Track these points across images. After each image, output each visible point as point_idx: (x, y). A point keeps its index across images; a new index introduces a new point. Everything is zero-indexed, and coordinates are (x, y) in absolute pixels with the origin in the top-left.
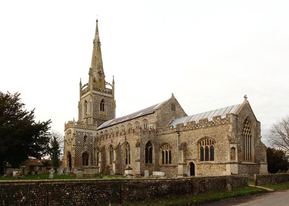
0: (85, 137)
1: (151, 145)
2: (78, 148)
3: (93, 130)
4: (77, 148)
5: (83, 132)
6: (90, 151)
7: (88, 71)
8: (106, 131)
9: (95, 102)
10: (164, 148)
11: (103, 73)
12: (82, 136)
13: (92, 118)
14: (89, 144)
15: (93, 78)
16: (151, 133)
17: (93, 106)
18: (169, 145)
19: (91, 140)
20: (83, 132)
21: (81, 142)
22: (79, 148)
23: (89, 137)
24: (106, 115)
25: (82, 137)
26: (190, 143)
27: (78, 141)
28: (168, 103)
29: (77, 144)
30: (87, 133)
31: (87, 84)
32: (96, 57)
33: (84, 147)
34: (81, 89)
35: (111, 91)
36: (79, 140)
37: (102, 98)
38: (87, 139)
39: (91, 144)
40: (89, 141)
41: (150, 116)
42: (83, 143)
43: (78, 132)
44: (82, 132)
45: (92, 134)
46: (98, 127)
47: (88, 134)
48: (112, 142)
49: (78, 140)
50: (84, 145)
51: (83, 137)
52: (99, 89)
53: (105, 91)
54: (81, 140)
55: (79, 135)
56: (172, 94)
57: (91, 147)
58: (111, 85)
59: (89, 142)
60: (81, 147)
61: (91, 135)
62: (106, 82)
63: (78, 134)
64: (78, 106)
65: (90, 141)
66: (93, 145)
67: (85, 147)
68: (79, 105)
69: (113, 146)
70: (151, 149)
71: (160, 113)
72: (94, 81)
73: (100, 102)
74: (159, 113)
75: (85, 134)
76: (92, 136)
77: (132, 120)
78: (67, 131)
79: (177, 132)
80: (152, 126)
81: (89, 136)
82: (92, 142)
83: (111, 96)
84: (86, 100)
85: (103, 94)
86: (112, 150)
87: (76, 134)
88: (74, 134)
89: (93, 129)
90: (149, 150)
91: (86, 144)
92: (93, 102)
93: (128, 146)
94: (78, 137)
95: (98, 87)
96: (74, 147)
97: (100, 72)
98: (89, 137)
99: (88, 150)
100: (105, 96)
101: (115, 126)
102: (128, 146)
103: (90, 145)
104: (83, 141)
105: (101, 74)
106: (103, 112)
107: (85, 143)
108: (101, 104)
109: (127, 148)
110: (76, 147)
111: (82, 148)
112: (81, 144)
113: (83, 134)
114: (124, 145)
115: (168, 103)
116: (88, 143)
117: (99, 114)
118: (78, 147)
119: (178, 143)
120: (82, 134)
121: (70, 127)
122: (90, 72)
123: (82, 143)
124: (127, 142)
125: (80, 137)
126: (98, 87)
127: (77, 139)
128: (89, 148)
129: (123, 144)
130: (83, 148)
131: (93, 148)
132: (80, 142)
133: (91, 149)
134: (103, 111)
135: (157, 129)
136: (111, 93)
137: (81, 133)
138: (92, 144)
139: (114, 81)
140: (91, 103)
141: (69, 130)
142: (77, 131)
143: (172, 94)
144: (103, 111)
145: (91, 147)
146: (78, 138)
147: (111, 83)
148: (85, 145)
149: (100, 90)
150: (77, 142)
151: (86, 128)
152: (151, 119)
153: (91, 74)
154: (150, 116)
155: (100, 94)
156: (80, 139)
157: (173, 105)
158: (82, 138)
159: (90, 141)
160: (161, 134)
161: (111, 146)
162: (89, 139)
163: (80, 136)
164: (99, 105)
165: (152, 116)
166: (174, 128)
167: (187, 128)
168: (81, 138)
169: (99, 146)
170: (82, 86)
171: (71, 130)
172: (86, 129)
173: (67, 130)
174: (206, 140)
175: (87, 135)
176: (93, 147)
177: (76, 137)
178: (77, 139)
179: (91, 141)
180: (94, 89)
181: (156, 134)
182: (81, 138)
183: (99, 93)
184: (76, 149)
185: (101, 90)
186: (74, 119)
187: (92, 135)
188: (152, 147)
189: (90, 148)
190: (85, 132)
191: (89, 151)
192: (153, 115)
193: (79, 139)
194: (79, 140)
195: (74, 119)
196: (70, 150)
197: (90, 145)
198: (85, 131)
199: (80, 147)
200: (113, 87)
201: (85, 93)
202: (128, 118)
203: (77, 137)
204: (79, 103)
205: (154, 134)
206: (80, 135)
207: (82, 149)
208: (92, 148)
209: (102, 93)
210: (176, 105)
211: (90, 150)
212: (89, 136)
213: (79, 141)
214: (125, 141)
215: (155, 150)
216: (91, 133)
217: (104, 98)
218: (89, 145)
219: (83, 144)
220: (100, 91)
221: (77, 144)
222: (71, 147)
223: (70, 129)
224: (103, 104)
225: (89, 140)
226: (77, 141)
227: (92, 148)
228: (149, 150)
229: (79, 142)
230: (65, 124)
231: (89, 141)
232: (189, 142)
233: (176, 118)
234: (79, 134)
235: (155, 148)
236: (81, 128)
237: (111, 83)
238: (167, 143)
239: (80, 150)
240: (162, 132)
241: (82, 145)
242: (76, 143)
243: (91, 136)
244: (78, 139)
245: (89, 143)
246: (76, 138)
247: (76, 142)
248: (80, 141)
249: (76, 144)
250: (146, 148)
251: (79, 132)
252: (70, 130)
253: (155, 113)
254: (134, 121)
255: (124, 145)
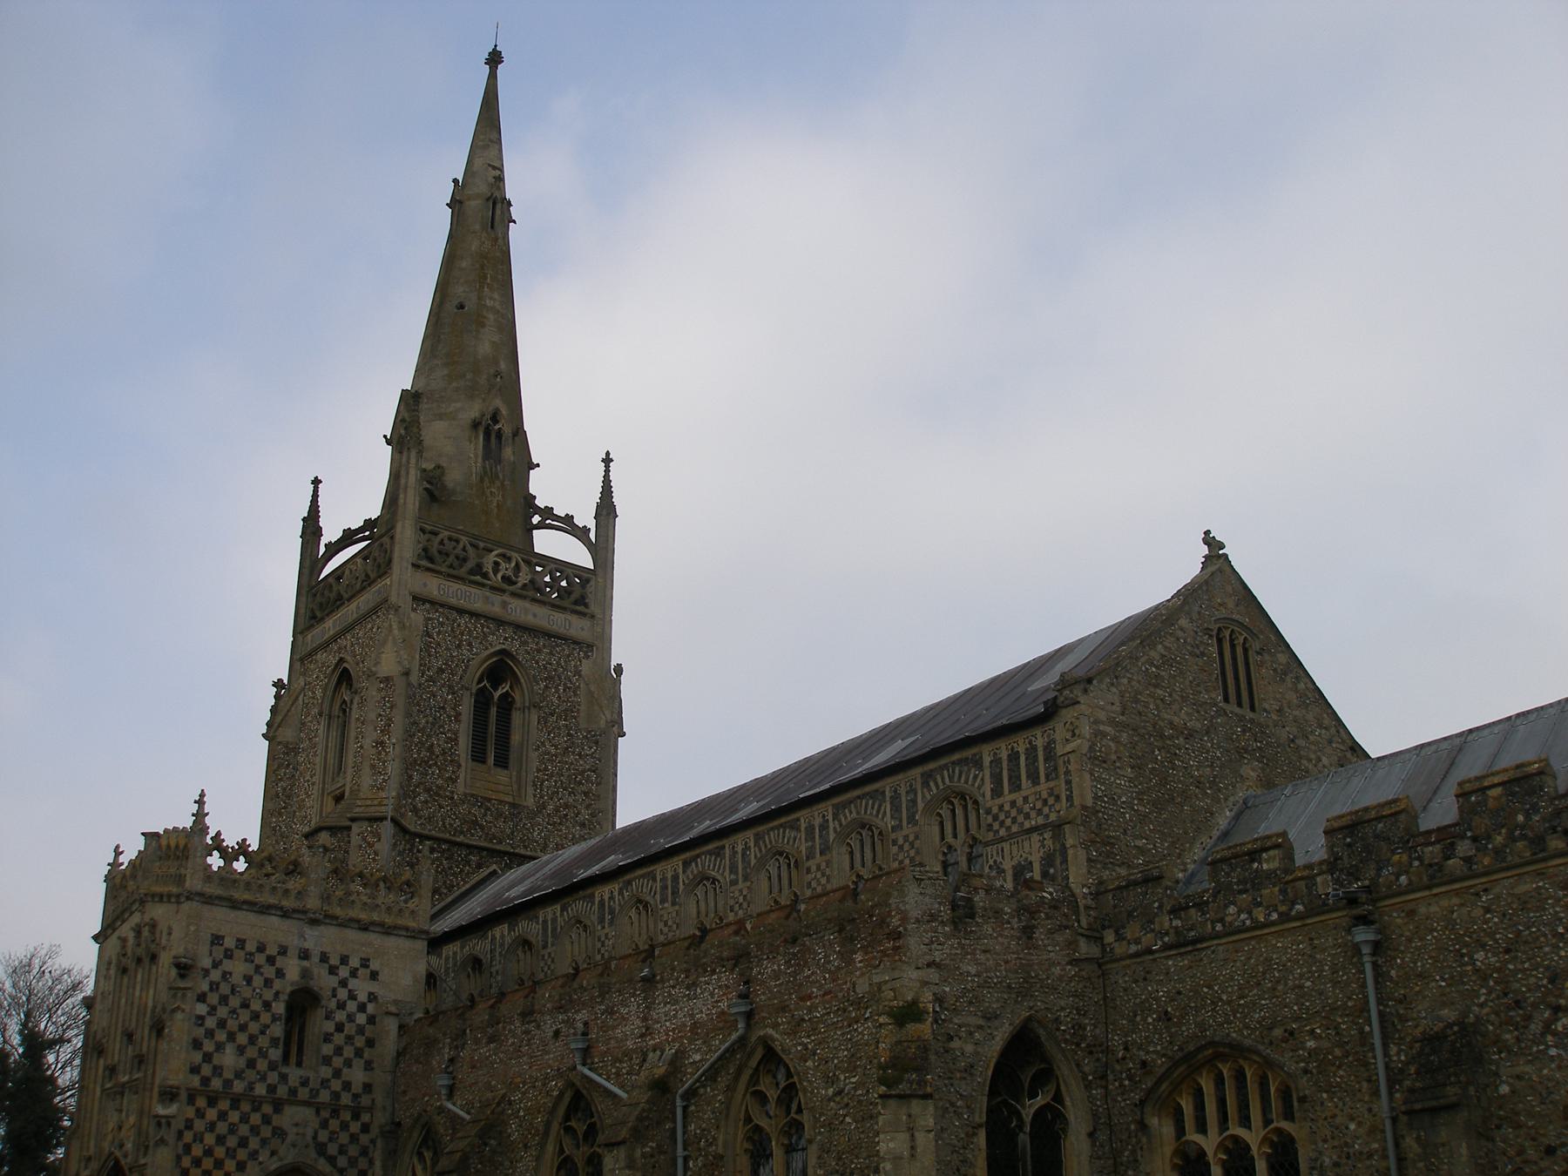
0: (303, 1002)
1: (1045, 1076)
2: (211, 1127)
3: (388, 930)
4: (199, 1125)
5: (283, 951)
6: (342, 1162)
7: (384, 418)
8: (526, 944)
9: (431, 679)
10: (1200, 1107)
11: (519, 434)
12: (268, 995)
13: (387, 829)
14: (336, 1085)
15: (429, 466)
16: (1039, 934)
17: (408, 715)
18: (1268, 1063)
19: (360, 1042)
20: (283, 951)
21: (251, 1064)
22: (222, 1128)
23: (341, 1006)
24: (530, 802)
25: (267, 1005)
26: (1535, 1027)
27: (220, 1047)
28: (1183, 622)
29: (205, 1081)
30: (324, 958)
31: (369, 524)
32: (461, 307)
33: (276, 1120)
34: (310, 561)
35: (585, 582)
36: (231, 1037)
37: (498, 641)
38: (319, 1024)
39: (357, 1087)
40: (339, 1051)
41: (1014, 757)
42: (273, 1066)
43: (229, 942)
44: (272, 950)
45: (374, 976)
46: (434, 917)
47: (333, 971)
48: (586, 1053)
49: (221, 1036)
50: (282, 1091)
51: (279, 1008)
52: (470, 564)
53: (524, 578)
54: (252, 1040)
55: (237, 979)
56: (1208, 539)
57: (356, 1116)
58: (581, 533)
59: (338, 1062)
60: (245, 1119)
61: (362, 988)
62: (538, 510)
63: (227, 965)
64: (268, 716)
65: (348, 1052)
66: (379, 1096)
67: (290, 1116)
68: (274, 710)
69: (600, 1105)
70: (1050, 1126)
71: (1111, 722)
72: (434, 491)
73: (477, 668)
74: (1102, 716)
75: (305, 974)
76: (372, 997)
77: (803, 816)
78: (124, 940)
79: (1352, 901)
80: (1036, 859)
81: (343, 994)
82: (369, 1066)
83: (576, 627)
84: (341, 660)
85: (504, 605)
86: (579, 1155)
87: (206, 962)
88: (183, 969)
89: (389, 920)
90: (1024, 1139)
91: (305, 1083)
92: (407, 674)
93: (772, 1094)
94: (224, 1000)
95: (464, 539)
96: (172, 1109)
97: (495, 418)
98: (341, 1006)
99: (321, 1149)
100: (520, 628)
101: (615, 887)
102: (772, 1094)
103: (346, 1099)
104: (274, 1042)
105: (499, 434)
106: (502, 776)
107: (294, 1074)
108: (482, 702)
109: (763, 1122)
110: (190, 1112)
111: (255, 1130)
112: (251, 1075)
113: (280, 974)
114: (723, 1081)
115: (1183, 622)
116: (326, 1072)
117: (461, 788)
118: (212, 1114)
119: (1377, 1041)
120: (270, 972)
121: (157, 889)
122: (399, 421)
123: (262, 1065)
124: (766, 1043)
125: (245, 1005)
126: (464, 539)
127: (211, 1023)
128: (334, 1124)
129: (712, 1073)
130: (266, 1132)
131: (375, 1131)
132: (242, 1063)
133: (354, 1138)
134: (502, 762)
135: (1096, 895)
136: (581, 600)
137: (260, 959)
138: (368, 1088)
139: (617, 500)
140: (387, 680)
141: (138, 931)
142: (217, 940)
143: (1208, 539)
144: (502, 762)
145: (356, 1116)
146: (223, 1012)
147: (586, 518)
148: (293, 1092)
149: (478, 569)
150: (208, 1058)
151: (313, 903)
152: (1016, 787)
153: (404, 437)
154: (1004, 755)
155: (478, 606)
156: (243, 1028)
157: (1233, 646)
158: (265, 1018)
159: (348, 1052)
160: (1147, 939)
161: (578, 1101)
162: (340, 1028)
163: (247, 992)
164: (467, 708)
165: (1032, 751)
166: (1300, 860)
167: (1464, 848)
168: (256, 1016)
169: (441, 1110)
170: (324, 541)
171: (162, 926)
172: (314, 922)
173: (126, 930)
174: (1219, 1081)
175: (324, 981)
176: (380, 1118)
177: (202, 998)
178: (211, 1023)
179: (359, 1053)
180: (428, 560)
181: (1095, 951)
182: (256, 1016)
183: (474, 598)
184: (188, 1137)
185: (488, 568)
186: (200, 802)
187: (373, 987)
188: (1058, 1097)
189: (345, 1126)
190: (305, 955)
191: (332, 1160)
192: (1040, 743)
193: (232, 1024)
194: (231, 1037)
195: (200, 802)
196: (129, 1146)
197: (346, 1099)
198: (302, 936)
199: (234, 1117)
200: (602, 547)
201: (339, 601)
202: (755, 805)
203: (213, 999)
204: (277, 697)
205: (1072, 944)
206: (249, 980)
207: (254, 1143)
208: (365, 1128)
209: (497, 598)
210: (1256, 646)
211: (342, 1150)
212: (343, 994)
213: (230, 1049)
214: (742, 1040)
215: (1091, 1135)
216: (365, 963)
217: (514, 647)
218: (336, 1095)
219: (273, 1078)
220: (485, 576)
221: (205, 1081)
222: (141, 1113)
223: (158, 911)
224: (505, 696)
225: (339, 1039)
226: (209, 1046)
227: (365, 1128)
228: (1024, 1139)
229: (229, 1059)
230: (114, 865)
231: (339, 1051)
232: (1516, 1014)
233: (1268, 784)
234: (238, 968)
235: (1095, 1115)
236: (265, 910)
237: (586, 518)
238: (1236, 1050)
239: (231, 1153)
240: (1165, 921)
241: (260, 1090)
242: (195, 1070)
243: (362, 997)
244: (222, 1024)
245: (337, 1074)
246: (202, 1009)
247: (197, 1057)
248: (241, 1050)
249: (196, 1081)
250: (990, 1111)
251: (241, 943)
252: (153, 926)
253: (1067, 714)
254: (824, 826)
255: (730, 1089)
